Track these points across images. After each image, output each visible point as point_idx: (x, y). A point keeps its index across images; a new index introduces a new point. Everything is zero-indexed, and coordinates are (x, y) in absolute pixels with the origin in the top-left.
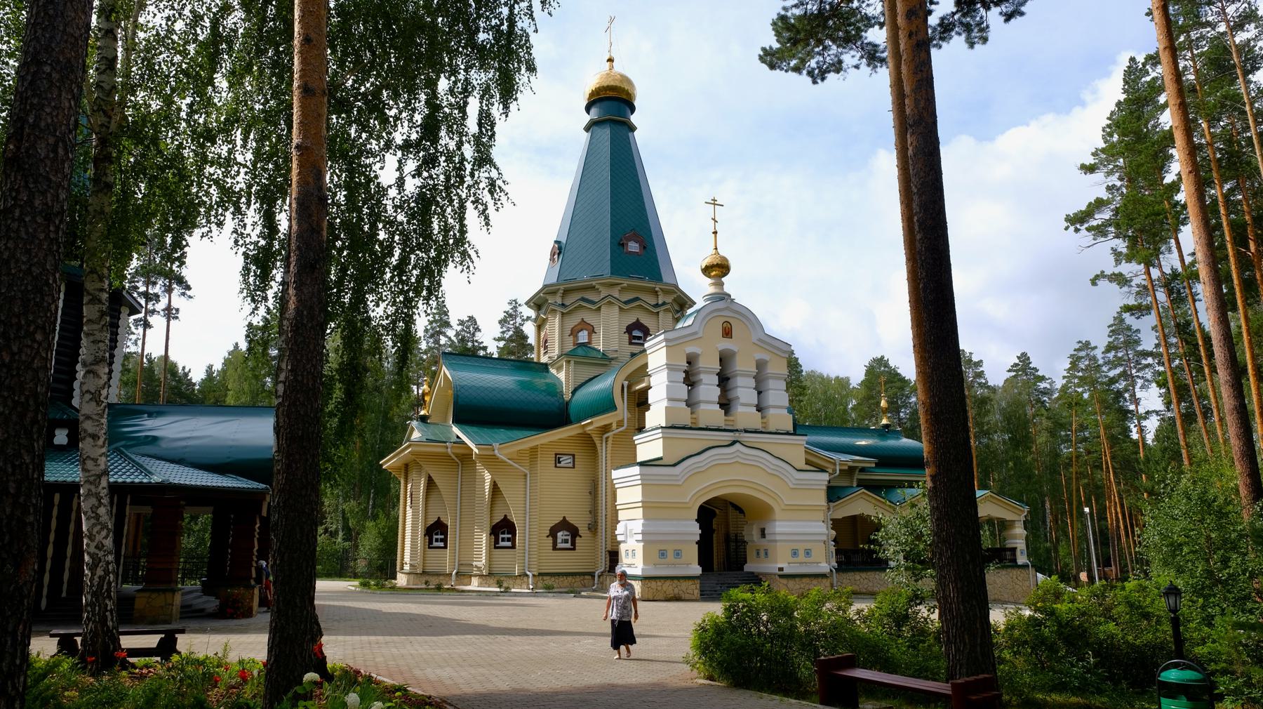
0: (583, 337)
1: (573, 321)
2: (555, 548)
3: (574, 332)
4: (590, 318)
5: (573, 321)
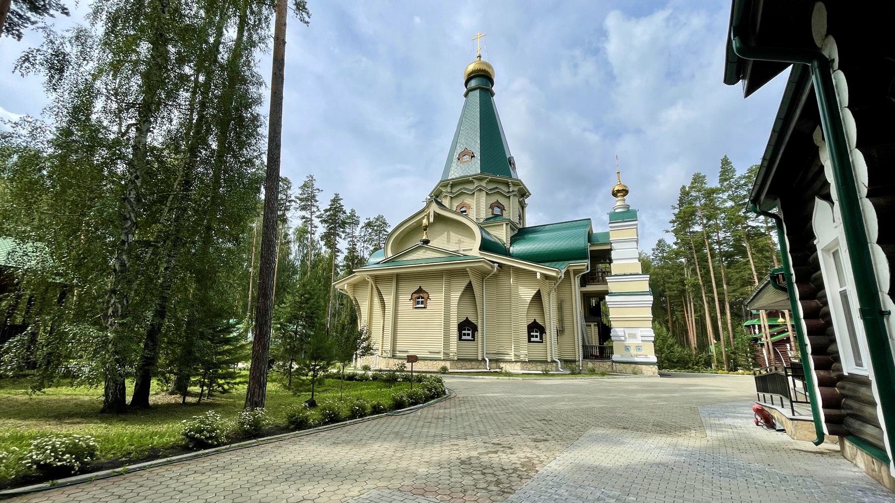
0: (497, 211)
1: (493, 200)
2: (529, 341)
3: (492, 207)
4: (503, 201)
5: (493, 200)
